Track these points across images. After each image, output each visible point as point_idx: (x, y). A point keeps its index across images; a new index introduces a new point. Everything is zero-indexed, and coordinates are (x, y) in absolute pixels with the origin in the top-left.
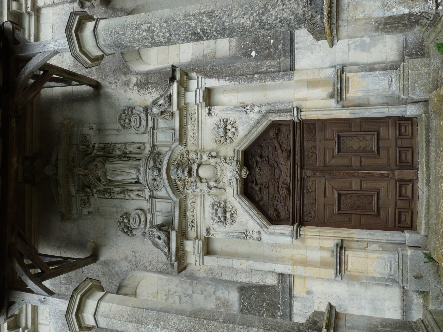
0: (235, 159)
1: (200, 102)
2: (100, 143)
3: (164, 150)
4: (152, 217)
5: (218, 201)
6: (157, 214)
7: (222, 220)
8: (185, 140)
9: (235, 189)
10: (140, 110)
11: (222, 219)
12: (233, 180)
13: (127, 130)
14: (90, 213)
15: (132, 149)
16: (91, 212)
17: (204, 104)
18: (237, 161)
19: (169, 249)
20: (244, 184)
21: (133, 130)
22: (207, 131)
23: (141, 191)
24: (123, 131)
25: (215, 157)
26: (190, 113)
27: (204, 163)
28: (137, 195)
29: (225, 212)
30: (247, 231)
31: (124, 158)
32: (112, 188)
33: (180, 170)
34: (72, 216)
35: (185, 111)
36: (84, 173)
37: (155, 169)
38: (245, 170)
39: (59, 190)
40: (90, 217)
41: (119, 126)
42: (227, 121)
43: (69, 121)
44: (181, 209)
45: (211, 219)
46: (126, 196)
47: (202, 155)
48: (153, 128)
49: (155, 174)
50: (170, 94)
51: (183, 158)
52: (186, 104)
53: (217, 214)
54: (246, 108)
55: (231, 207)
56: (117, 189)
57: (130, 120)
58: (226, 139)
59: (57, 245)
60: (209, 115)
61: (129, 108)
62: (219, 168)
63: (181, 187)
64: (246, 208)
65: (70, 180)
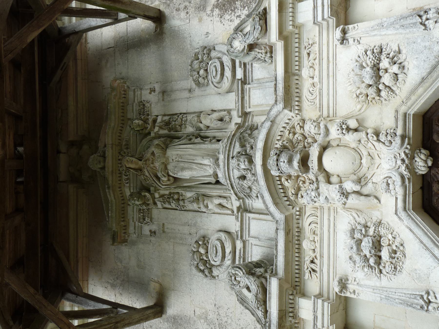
0: (399, 132)
1: (323, 19)
2: (165, 115)
3: (258, 120)
4: (244, 247)
5: (363, 222)
6: (252, 241)
7: (372, 264)
8: (297, 99)
9: (400, 198)
10: (223, 50)
11: (372, 261)
12: (394, 178)
13: (203, 89)
14: (153, 233)
15: (209, 121)
16: (155, 233)
17: (332, 21)
18: (403, 137)
19: (266, 312)
20: (422, 188)
21: (211, 89)
22: (340, 78)
23: (225, 197)
24: (197, 91)
25: (356, 130)
26: (306, 44)
27: (334, 143)
28: (220, 204)
29: (377, 245)
30: (428, 293)
31: (196, 138)
32: (180, 191)
33: (284, 158)
34: (129, 236)
35: (297, 40)
36: (137, 167)
37: (242, 157)
38: (423, 157)
39: (108, 193)
40: (153, 239)
41: (190, 83)
42: (381, 52)
43: (122, 81)
44: (290, 236)
45: (348, 259)
46: (202, 206)
47: (329, 126)
48: (244, 82)
49: (243, 166)
50: (265, 9)
51: (294, 134)
52: (299, 27)
53: (359, 250)
54: (424, 18)
55: (390, 237)
56: (189, 195)
57: (206, 70)
58: (379, 91)
59: (110, 281)
60: (342, 43)
61: (206, 47)
62: (365, 153)
63: (291, 192)
64: (426, 240)
65: (124, 177)
